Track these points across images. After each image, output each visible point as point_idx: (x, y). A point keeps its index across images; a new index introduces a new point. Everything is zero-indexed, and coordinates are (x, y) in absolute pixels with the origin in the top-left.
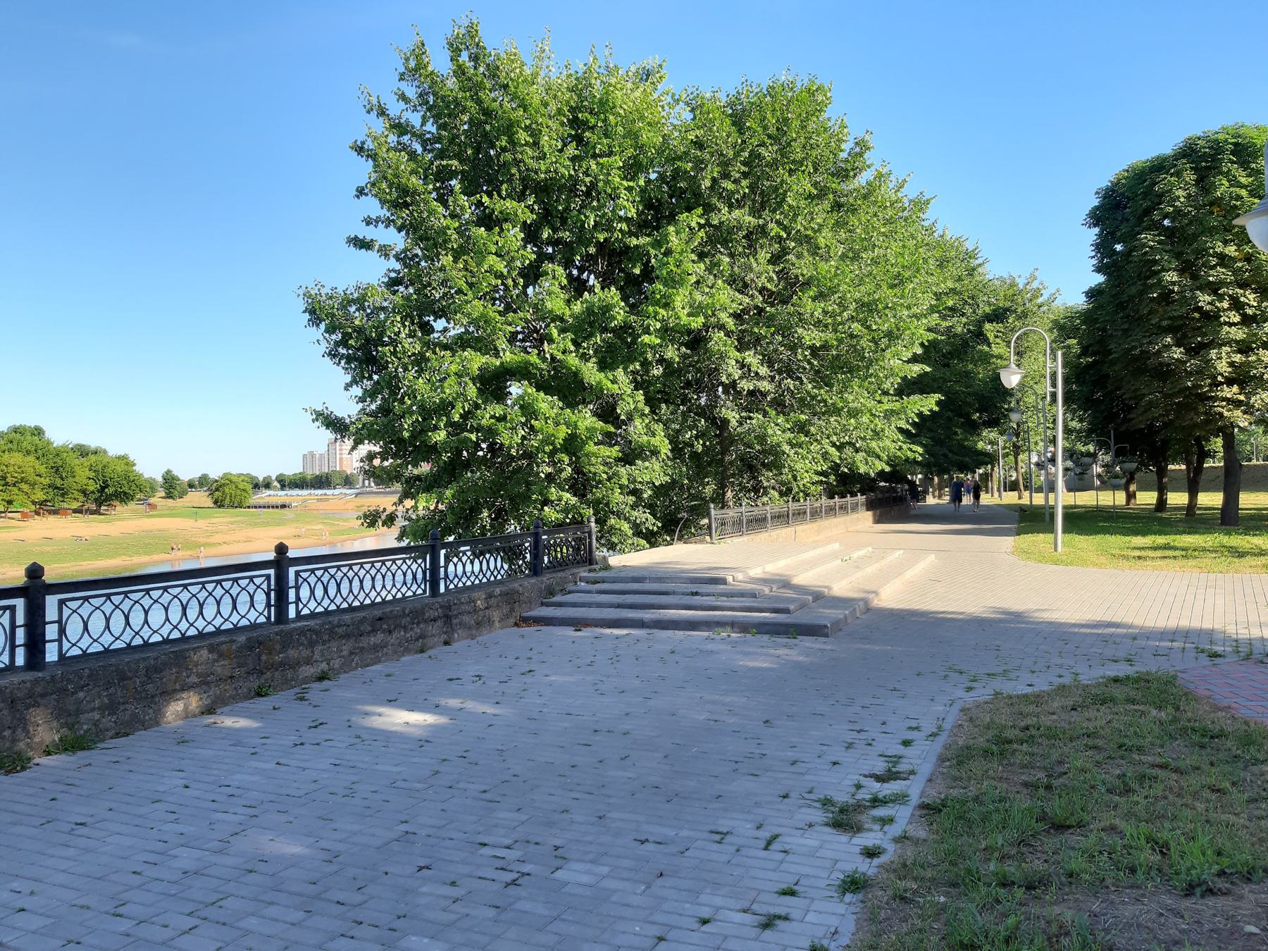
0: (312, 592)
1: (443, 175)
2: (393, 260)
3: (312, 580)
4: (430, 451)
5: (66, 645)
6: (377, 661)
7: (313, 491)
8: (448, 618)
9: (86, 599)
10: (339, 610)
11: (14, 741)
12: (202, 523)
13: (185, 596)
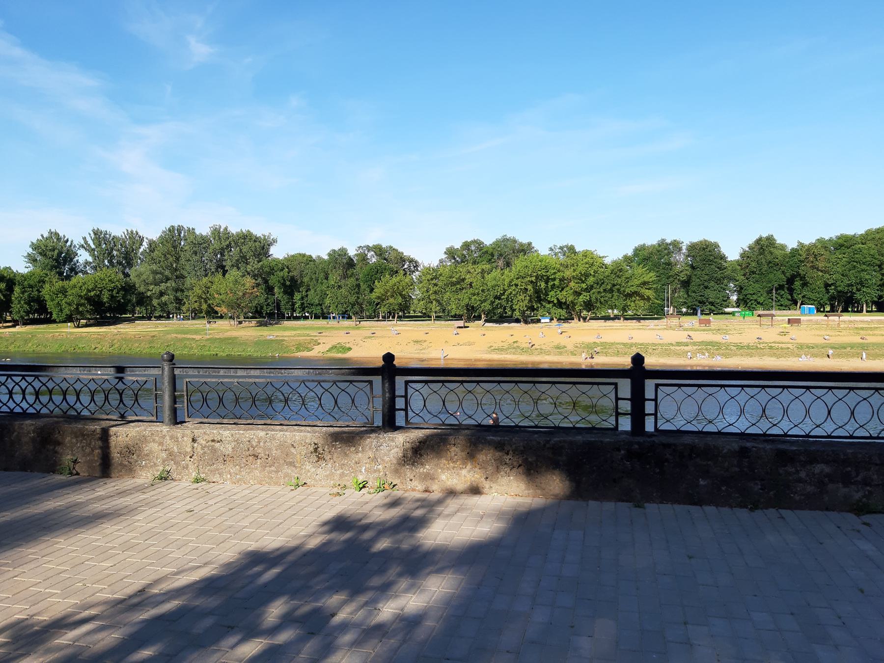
5: (410, 414)
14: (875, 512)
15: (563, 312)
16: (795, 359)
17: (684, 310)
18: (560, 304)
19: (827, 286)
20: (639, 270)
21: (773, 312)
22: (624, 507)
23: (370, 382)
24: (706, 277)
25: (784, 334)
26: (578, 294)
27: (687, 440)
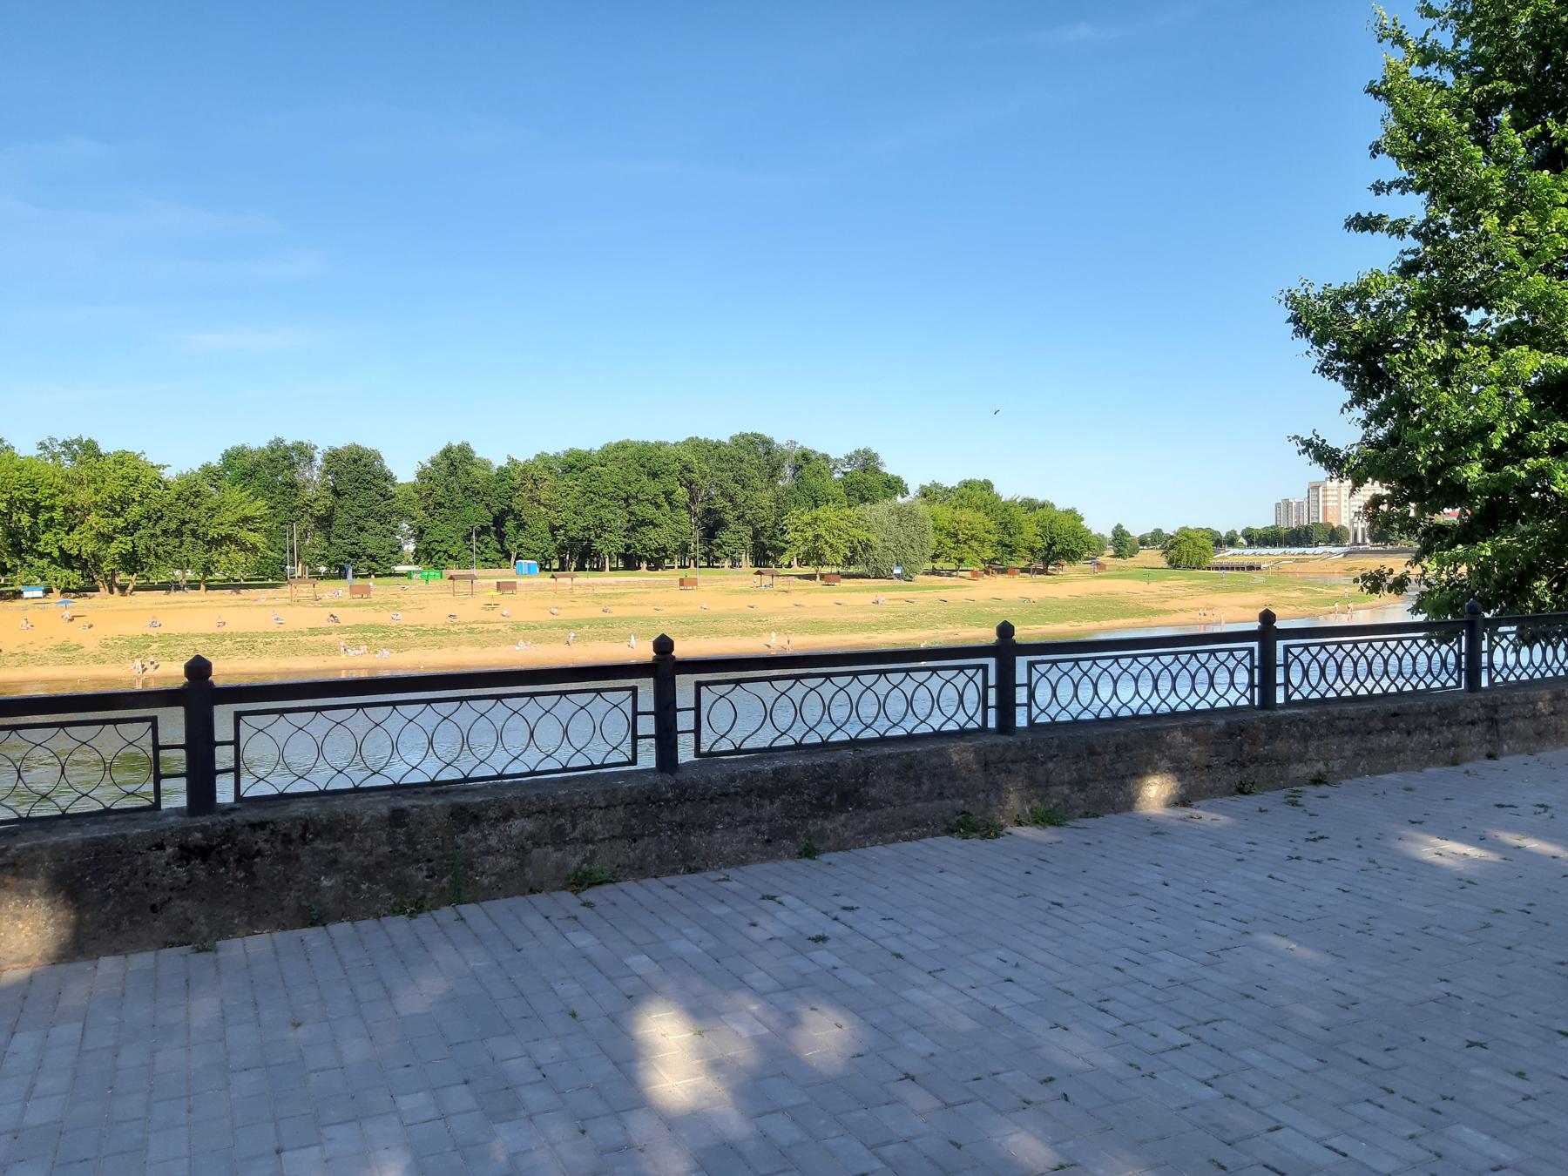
0: (1306, 673)
1: (1486, 109)
2: (1409, 237)
3: (1306, 657)
4: (1457, 494)
5: (1035, 711)
6: (1392, 769)
7: (1288, 550)
8: (1493, 722)
9: (1054, 662)
10: (1339, 699)
11: (988, 805)
12: (1155, 586)
13: (1156, 667)
14: (600, 883)
15: (75, 576)
16: (509, 648)
17: (323, 569)
18: (67, 560)
19: (554, 529)
20: (235, 495)
21: (474, 571)
22: (173, 958)
23: (634, 690)
24: (361, 512)
25: (490, 607)
26: (107, 539)
27: (298, 809)
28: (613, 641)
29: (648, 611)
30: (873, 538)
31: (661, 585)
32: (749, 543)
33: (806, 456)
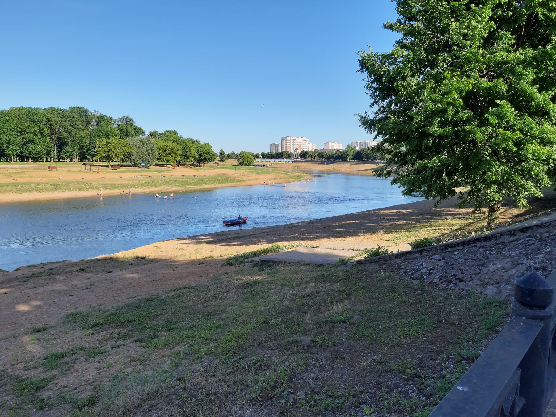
12: (237, 172)
28: (19, 193)
29: (35, 180)
30: (133, 151)
31: (38, 169)
32: (77, 151)
33: (102, 117)
